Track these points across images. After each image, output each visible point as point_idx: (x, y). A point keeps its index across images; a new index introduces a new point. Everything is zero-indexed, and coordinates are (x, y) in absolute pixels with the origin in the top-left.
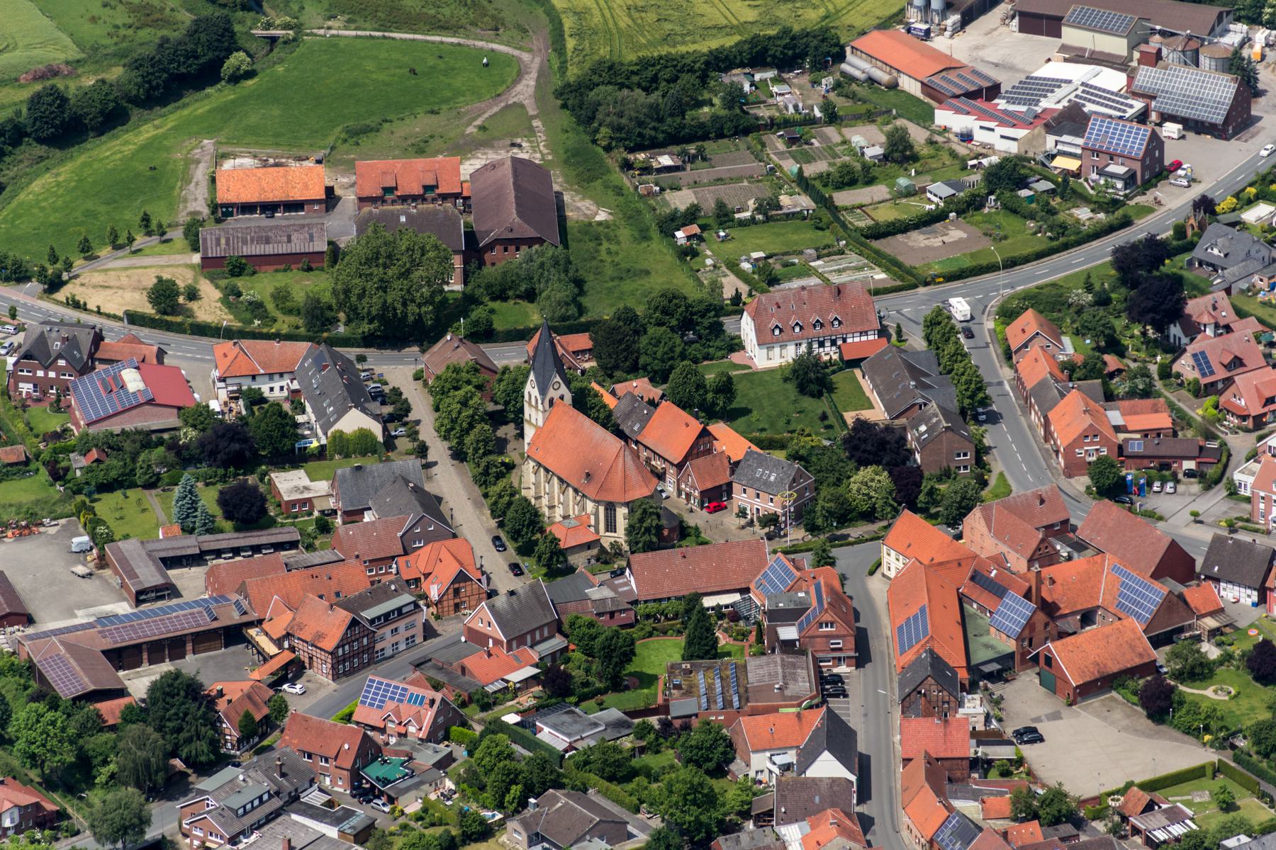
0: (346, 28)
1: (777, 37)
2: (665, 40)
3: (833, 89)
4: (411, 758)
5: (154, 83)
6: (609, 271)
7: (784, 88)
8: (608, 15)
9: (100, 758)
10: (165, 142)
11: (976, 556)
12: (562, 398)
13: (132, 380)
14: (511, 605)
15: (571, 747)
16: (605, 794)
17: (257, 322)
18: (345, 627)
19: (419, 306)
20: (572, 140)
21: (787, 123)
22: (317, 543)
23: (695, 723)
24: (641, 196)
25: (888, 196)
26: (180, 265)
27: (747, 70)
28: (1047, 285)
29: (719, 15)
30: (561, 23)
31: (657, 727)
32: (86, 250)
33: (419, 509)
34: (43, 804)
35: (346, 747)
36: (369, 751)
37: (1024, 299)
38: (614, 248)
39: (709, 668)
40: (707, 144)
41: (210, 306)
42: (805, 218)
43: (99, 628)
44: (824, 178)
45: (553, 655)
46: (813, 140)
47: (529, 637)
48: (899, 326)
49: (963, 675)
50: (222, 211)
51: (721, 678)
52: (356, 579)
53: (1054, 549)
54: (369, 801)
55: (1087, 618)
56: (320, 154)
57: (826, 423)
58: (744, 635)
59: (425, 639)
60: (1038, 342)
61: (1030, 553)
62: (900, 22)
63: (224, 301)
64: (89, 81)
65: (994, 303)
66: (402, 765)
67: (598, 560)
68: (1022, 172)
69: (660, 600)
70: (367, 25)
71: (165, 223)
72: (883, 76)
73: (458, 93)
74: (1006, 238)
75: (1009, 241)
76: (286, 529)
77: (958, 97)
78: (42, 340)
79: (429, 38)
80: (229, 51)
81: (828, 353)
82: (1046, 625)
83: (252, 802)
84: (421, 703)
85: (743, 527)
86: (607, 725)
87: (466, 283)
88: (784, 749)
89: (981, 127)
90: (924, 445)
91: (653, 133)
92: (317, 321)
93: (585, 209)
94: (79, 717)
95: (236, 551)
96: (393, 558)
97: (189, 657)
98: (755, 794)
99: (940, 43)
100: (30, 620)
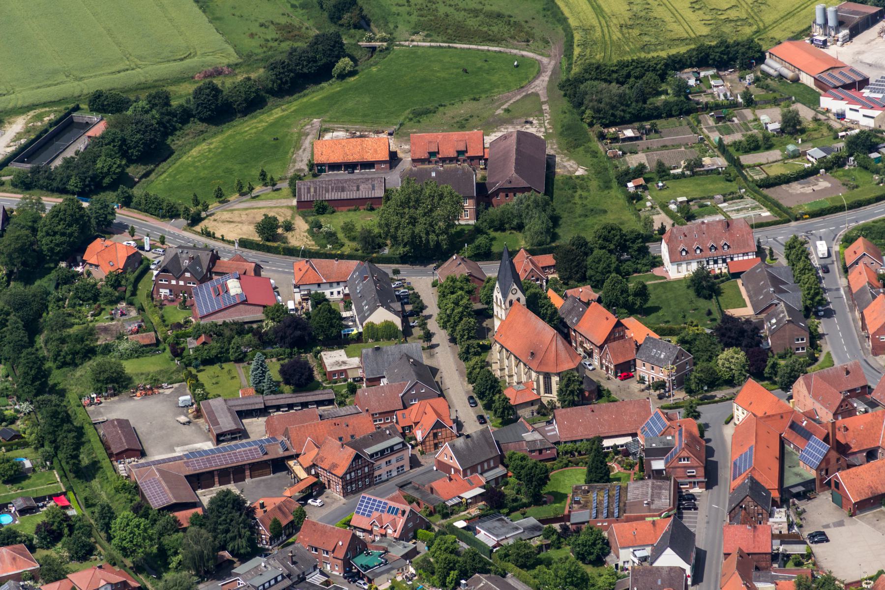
0: (424, 41)
1: (716, 47)
2: (643, 48)
3: (754, 83)
4: (387, 552)
5: (284, 80)
6: (579, 210)
7: (720, 82)
8: (606, 30)
9: (172, 550)
10: (287, 121)
11: (793, 412)
12: (518, 300)
13: (234, 287)
14: (467, 445)
15: (498, 544)
16: (518, 577)
17: (329, 246)
18: (351, 460)
19: (437, 235)
20: (567, 119)
21: (717, 106)
22: (348, 400)
23: (584, 527)
24: (609, 158)
25: (780, 158)
26: (280, 206)
27: (695, 70)
28: (880, 220)
29: (682, 29)
30: (572, 37)
31: (559, 531)
32: (220, 196)
33: (415, 377)
34: (129, 582)
35: (340, 543)
36: (357, 547)
37: (862, 230)
38: (584, 194)
39: (602, 489)
40: (658, 122)
41: (300, 236)
42: (719, 173)
43: (185, 460)
44: (737, 145)
45: (496, 479)
46: (734, 119)
47: (479, 468)
48: (771, 249)
49: (775, 494)
50: (317, 169)
51: (609, 496)
52: (365, 426)
53: (852, 406)
54: (355, 582)
55: (871, 454)
56: (391, 130)
57: (712, 317)
58: (631, 466)
59: (411, 468)
60: (866, 260)
61: (835, 409)
62: (808, 35)
63: (310, 232)
64: (240, 78)
65: (842, 233)
66: (380, 556)
67: (538, 413)
68: (874, 140)
69: (575, 441)
70: (439, 39)
71: (276, 178)
72: (789, 74)
73: (495, 86)
74: (857, 187)
75: (859, 189)
76: (326, 391)
77: (836, 88)
78: (176, 259)
79: (480, 47)
80: (338, 58)
81: (719, 268)
82: (838, 460)
83: (269, 582)
84: (396, 514)
85: (643, 390)
86: (525, 529)
87: (477, 220)
88: (643, 546)
89: (851, 109)
90: (773, 333)
91: (622, 114)
92: (370, 247)
93: (569, 166)
94: (162, 522)
95: (290, 406)
96: (394, 411)
97: (248, 480)
98: (618, 578)
99: (833, 51)
100: (142, 454)
